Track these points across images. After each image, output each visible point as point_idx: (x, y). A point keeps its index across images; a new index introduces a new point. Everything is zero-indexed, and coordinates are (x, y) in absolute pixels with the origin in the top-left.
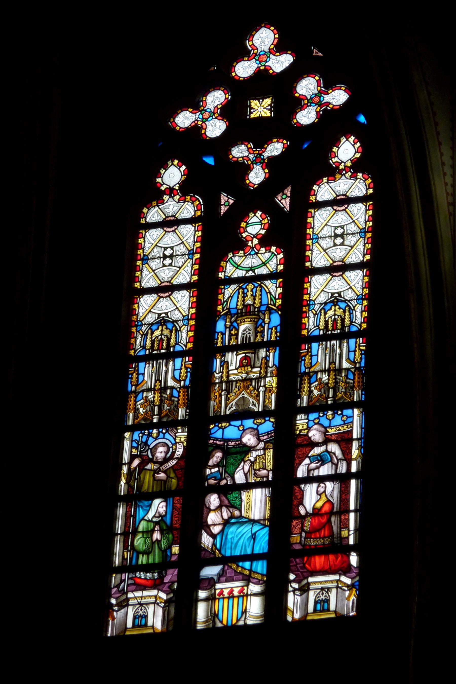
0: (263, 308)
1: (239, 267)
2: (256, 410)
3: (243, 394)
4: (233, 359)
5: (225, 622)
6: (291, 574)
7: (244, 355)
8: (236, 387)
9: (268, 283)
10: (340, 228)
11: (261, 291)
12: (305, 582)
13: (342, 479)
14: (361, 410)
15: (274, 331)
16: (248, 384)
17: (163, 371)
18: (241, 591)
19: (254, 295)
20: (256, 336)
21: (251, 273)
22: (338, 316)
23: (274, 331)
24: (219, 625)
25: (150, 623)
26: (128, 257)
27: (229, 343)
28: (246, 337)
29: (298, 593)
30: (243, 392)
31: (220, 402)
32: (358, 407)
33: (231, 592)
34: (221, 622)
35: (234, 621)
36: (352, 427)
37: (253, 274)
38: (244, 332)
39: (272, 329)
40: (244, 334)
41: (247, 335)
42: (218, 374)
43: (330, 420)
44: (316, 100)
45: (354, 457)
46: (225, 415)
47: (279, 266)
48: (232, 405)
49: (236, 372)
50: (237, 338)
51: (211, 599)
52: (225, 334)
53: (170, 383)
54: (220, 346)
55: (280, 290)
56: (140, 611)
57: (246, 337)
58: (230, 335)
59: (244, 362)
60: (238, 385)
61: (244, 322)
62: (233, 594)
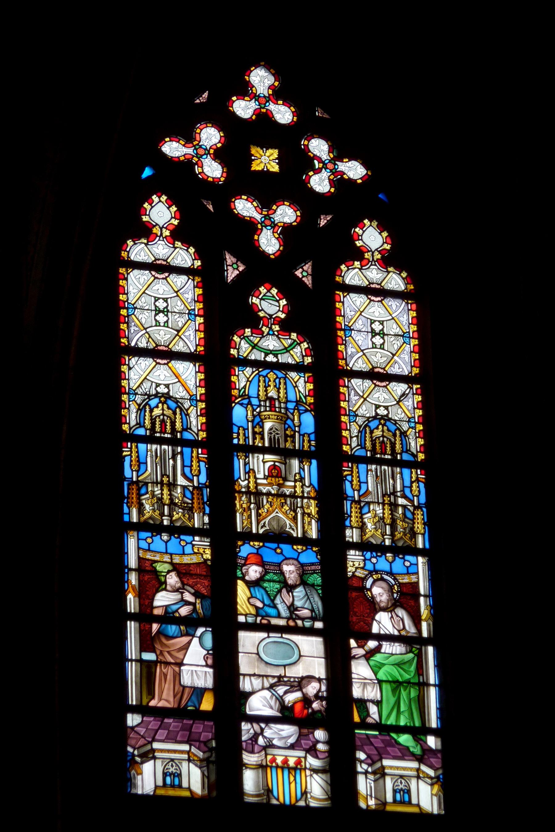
0: (291, 406)
1: (256, 347)
2: (295, 535)
3: (277, 512)
4: (261, 464)
5: (281, 799)
6: (367, 720)
7: (272, 463)
8: (268, 502)
9: (293, 375)
10: (379, 326)
11: (285, 384)
12: (378, 765)
13: (412, 642)
14: (427, 558)
15: (306, 439)
16: (283, 501)
17: (171, 465)
18: (298, 762)
19: (278, 386)
20: (286, 441)
21: (271, 358)
22: (388, 438)
23: (306, 439)
24: (274, 802)
25: (185, 784)
26: (109, 309)
27: (254, 443)
28: (274, 438)
29: (371, 777)
30: (277, 510)
31: (250, 517)
32: (423, 556)
33: (285, 761)
34: (278, 799)
35: (293, 801)
36: (418, 578)
37: (275, 360)
38: (271, 431)
39: (303, 435)
40: (271, 433)
41: (274, 435)
42: (243, 481)
43: (391, 563)
44: (268, 222)
45: (423, 618)
46: (257, 534)
47: (306, 358)
48: (265, 523)
49: (265, 481)
50: (263, 438)
51: (262, 767)
52: (248, 429)
53: (181, 481)
54: (242, 444)
55: (310, 386)
56: (170, 767)
57: (274, 438)
58: (254, 433)
59: (273, 471)
60: (269, 500)
61: (269, 418)
62: (288, 765)
